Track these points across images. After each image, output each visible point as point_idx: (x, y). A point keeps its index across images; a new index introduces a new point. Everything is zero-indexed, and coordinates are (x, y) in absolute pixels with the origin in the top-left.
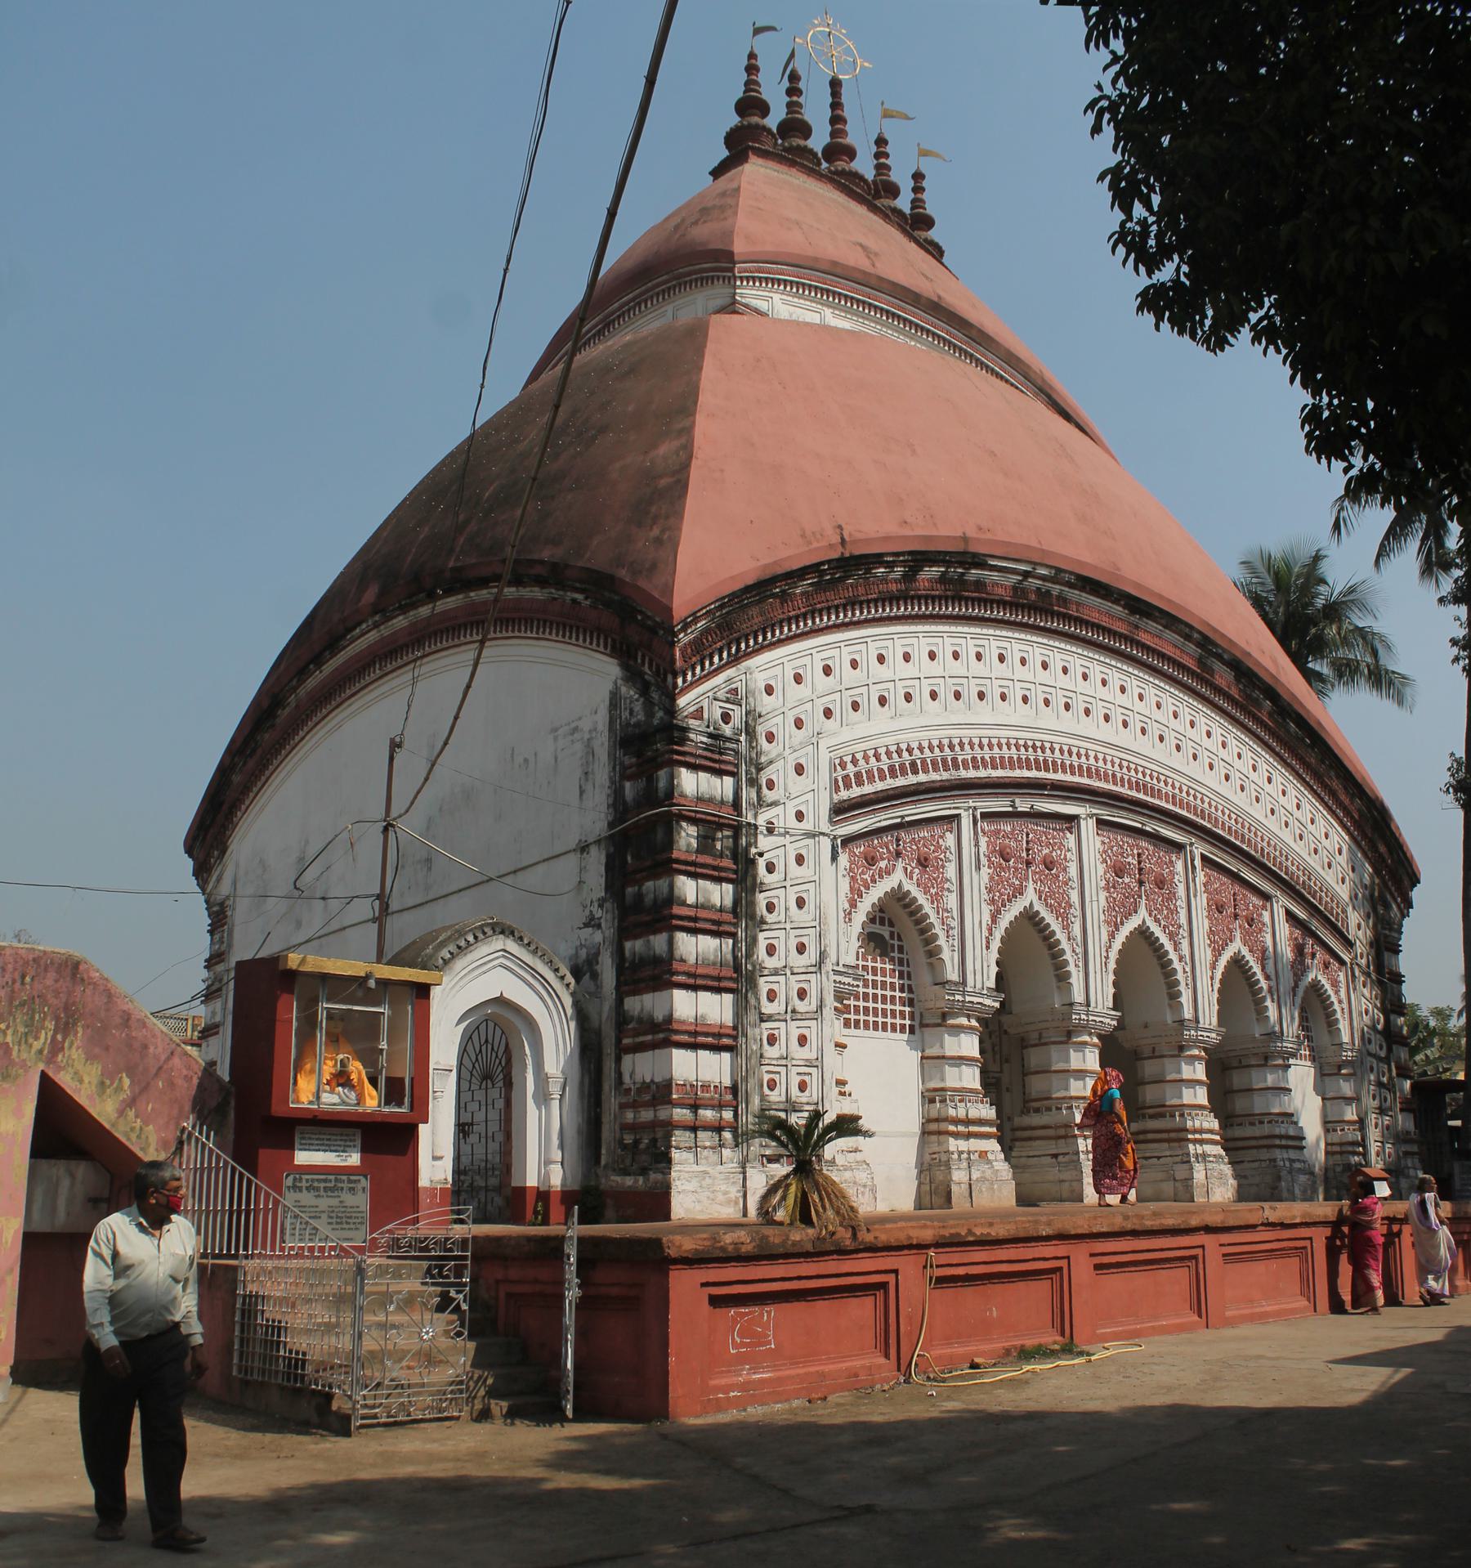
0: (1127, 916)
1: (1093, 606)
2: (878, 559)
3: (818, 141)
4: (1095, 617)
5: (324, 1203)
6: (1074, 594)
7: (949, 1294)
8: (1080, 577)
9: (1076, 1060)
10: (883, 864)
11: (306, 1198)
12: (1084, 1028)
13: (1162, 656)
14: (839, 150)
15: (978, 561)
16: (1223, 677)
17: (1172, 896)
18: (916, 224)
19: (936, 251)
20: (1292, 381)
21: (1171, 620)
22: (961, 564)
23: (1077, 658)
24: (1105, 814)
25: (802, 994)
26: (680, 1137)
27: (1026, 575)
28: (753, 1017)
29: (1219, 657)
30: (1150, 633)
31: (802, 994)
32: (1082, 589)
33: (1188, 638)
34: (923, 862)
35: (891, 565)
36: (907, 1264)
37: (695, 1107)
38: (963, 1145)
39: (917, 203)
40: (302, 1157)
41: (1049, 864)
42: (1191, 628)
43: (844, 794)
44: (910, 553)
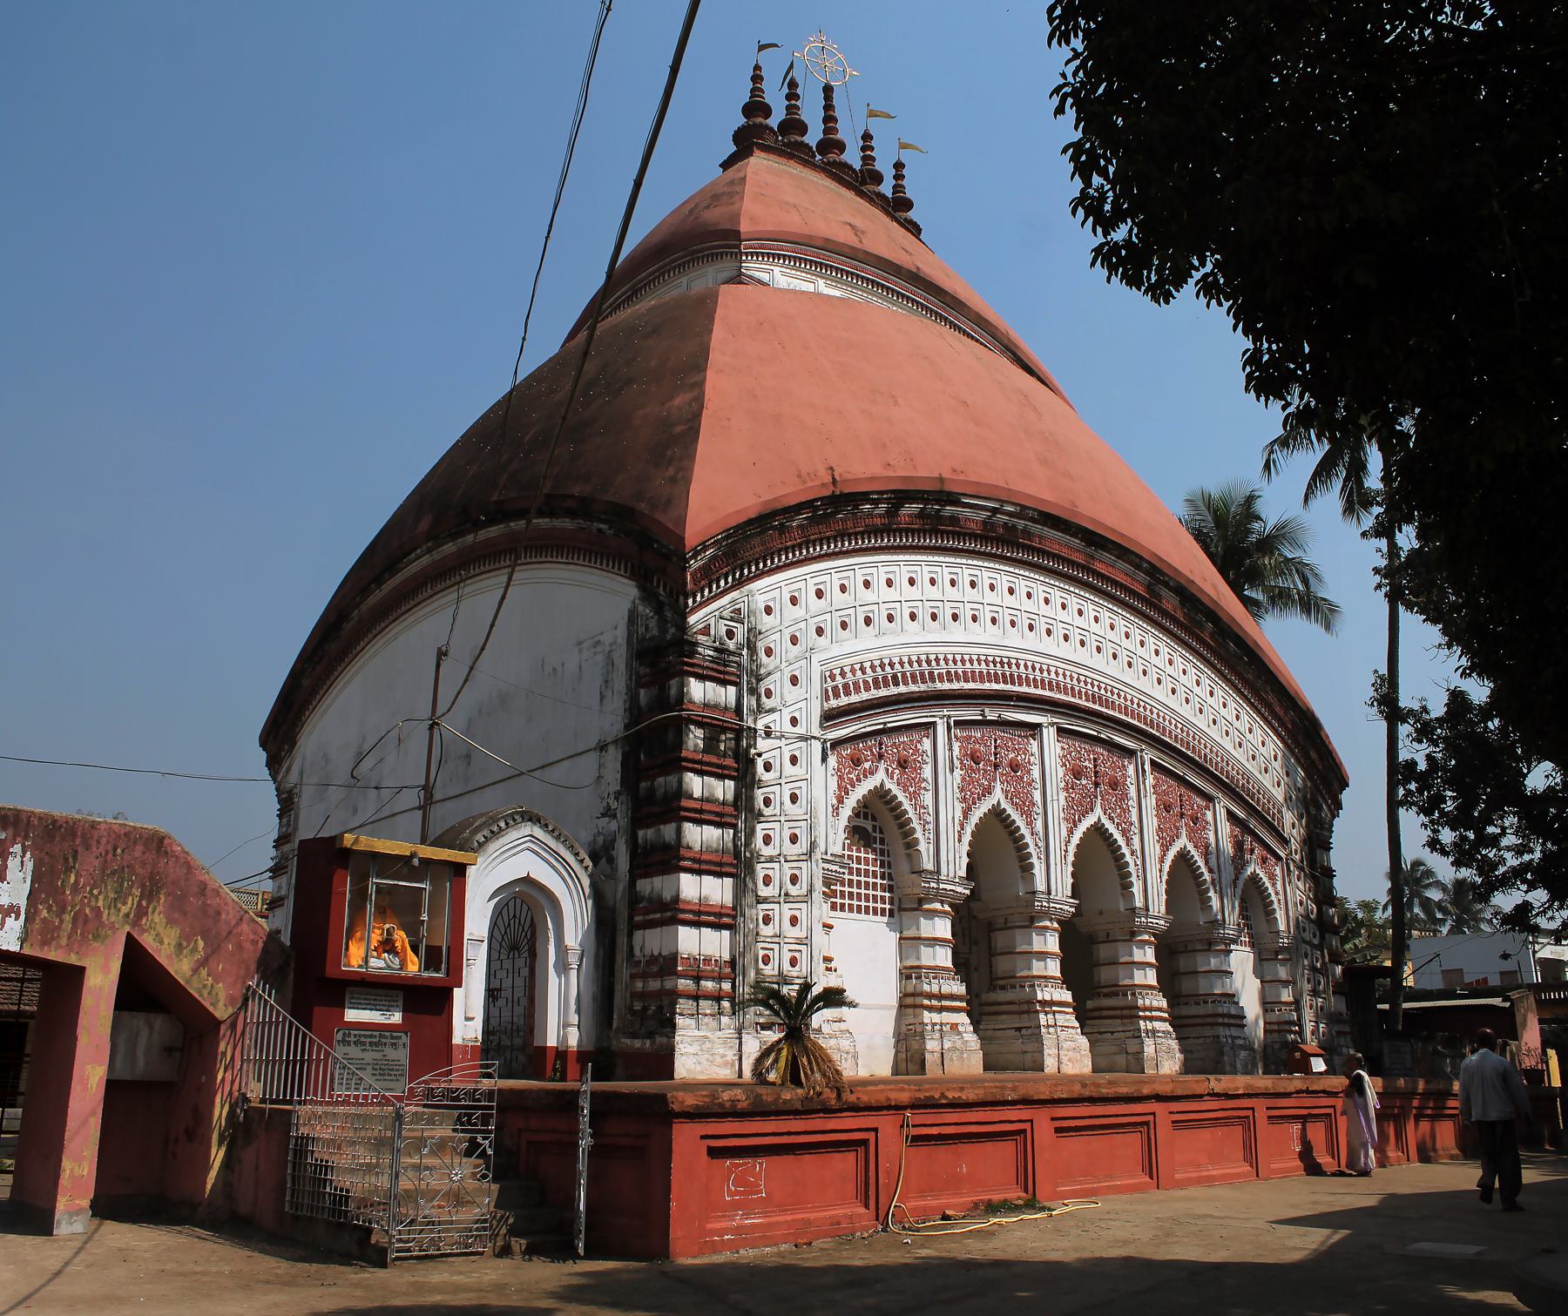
0: (1084, 814)
1: (1054, 539)
2: (864, 497)
3: (813, 137)
4: (1056, 549)
5: (369, 1056)
6: (1037, 528)
7: (923, 1151)
8: (1041, 513)
9: (1038, 943)
10: (867, 765)
11: (354, 1051)
12: (1046, 914)
13: (1115, 583)
14: (831, 144)
15: (953, 499)
16: (1170, 602)
17: (1125, 796)
18: (897, 207)
19: (914, 229)
20: (1093, 264)
21: (1122, 551)
22: (938, 502)
23: (1040, 585)
24: (1065, 723)
25: (794, 880)
26: (683, 1005)
27: (995, 511)
28: (750, 899)
29: (1166, 585)
30: (1105, 563)
31: (794, 880)
32: (1044, 524)
33: (1138, 567)
34: (903, 764)
35: (876, 502)
36: (886, 1124)
37: (697, 979)
38: (936, 1017)
39: (898, 188)
40: (352, 1015)
41: (1014, 767)
42: (1141, 558)
43: (834, 703)
44: (893, 492)
